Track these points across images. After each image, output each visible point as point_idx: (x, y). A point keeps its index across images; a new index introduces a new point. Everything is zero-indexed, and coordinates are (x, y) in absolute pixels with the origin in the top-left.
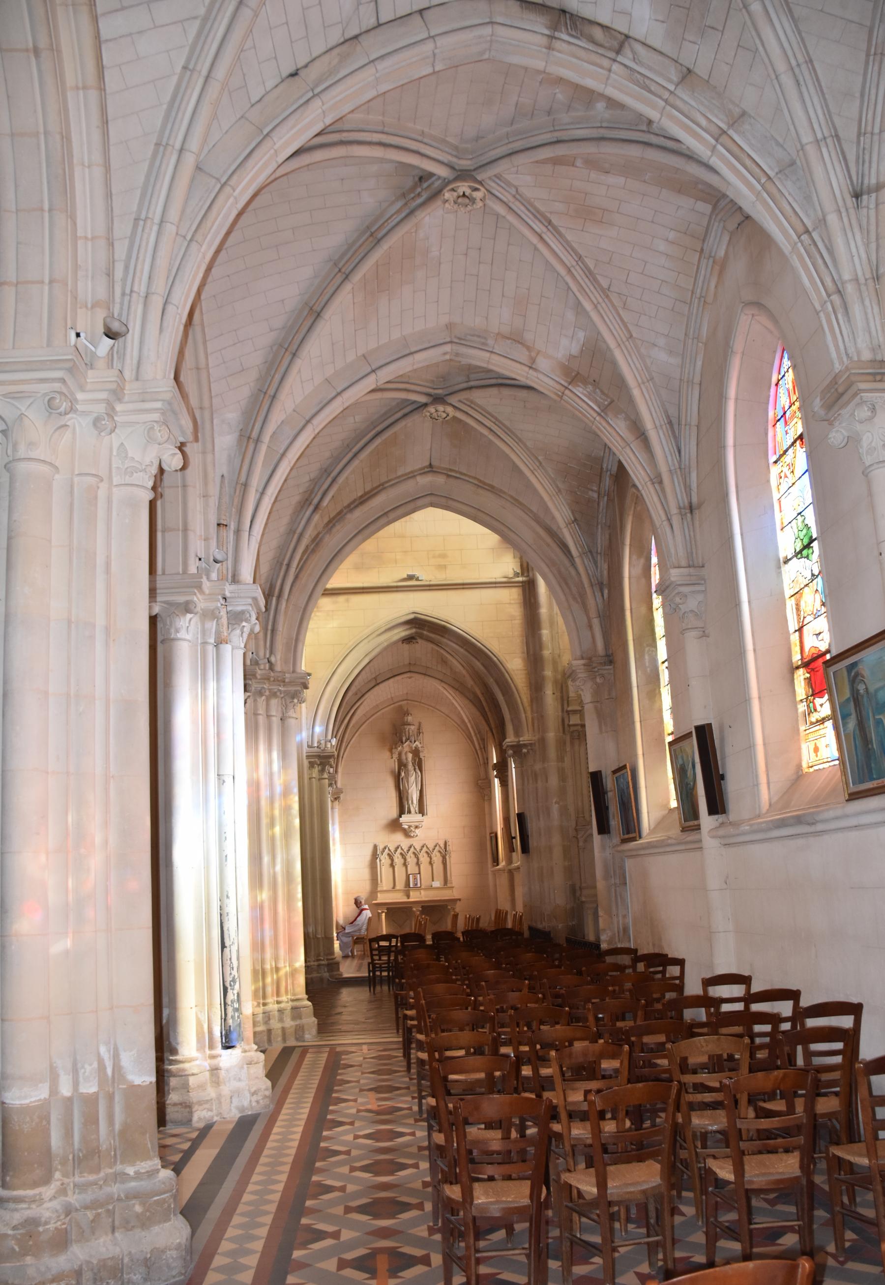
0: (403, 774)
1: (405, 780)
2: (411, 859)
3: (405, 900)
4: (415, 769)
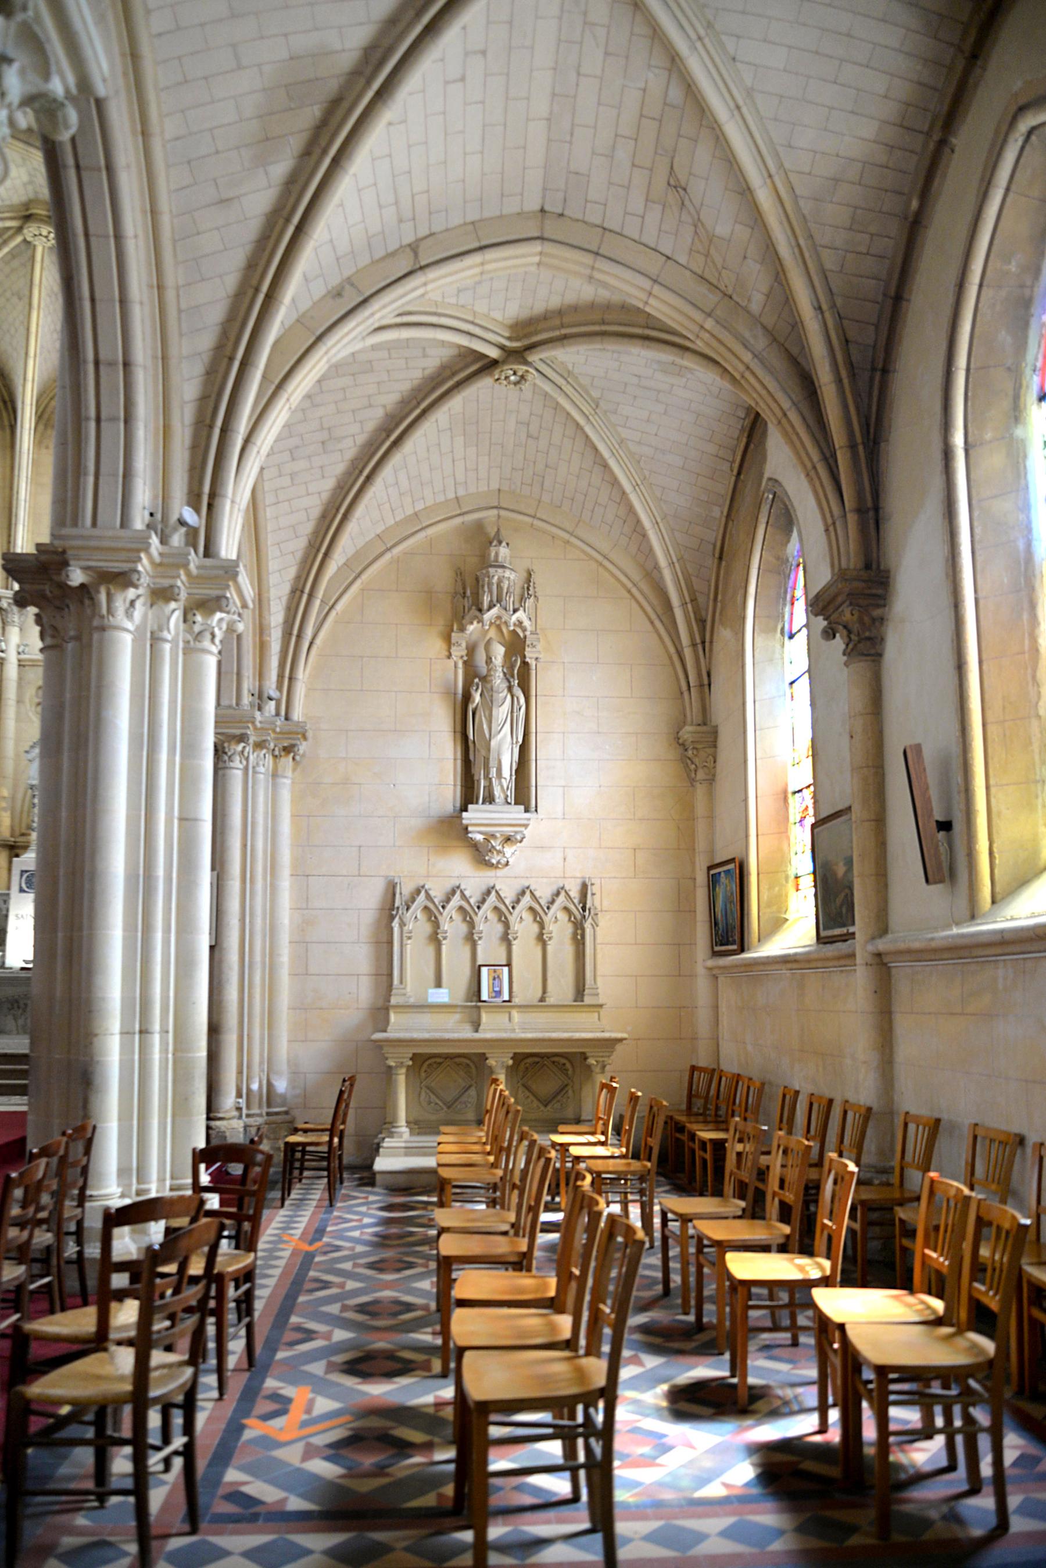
0: (477, 698)
1: (481, 715)
2: (488, 927)
3: (467, 1033)
4: (510, 689)
